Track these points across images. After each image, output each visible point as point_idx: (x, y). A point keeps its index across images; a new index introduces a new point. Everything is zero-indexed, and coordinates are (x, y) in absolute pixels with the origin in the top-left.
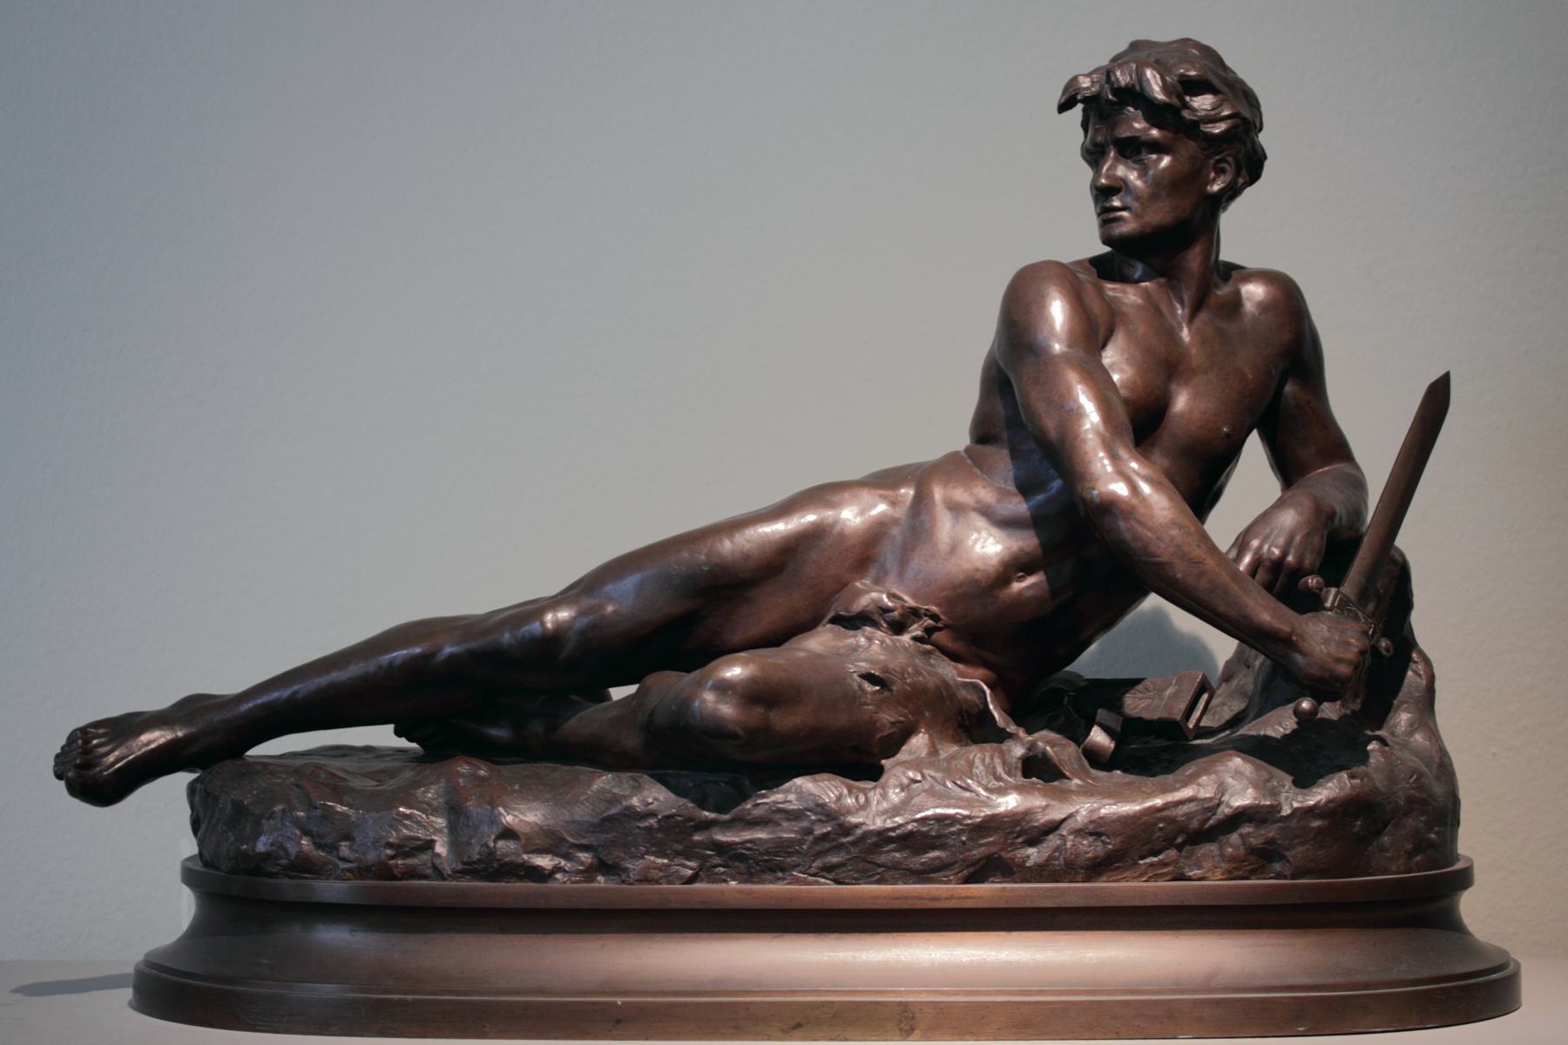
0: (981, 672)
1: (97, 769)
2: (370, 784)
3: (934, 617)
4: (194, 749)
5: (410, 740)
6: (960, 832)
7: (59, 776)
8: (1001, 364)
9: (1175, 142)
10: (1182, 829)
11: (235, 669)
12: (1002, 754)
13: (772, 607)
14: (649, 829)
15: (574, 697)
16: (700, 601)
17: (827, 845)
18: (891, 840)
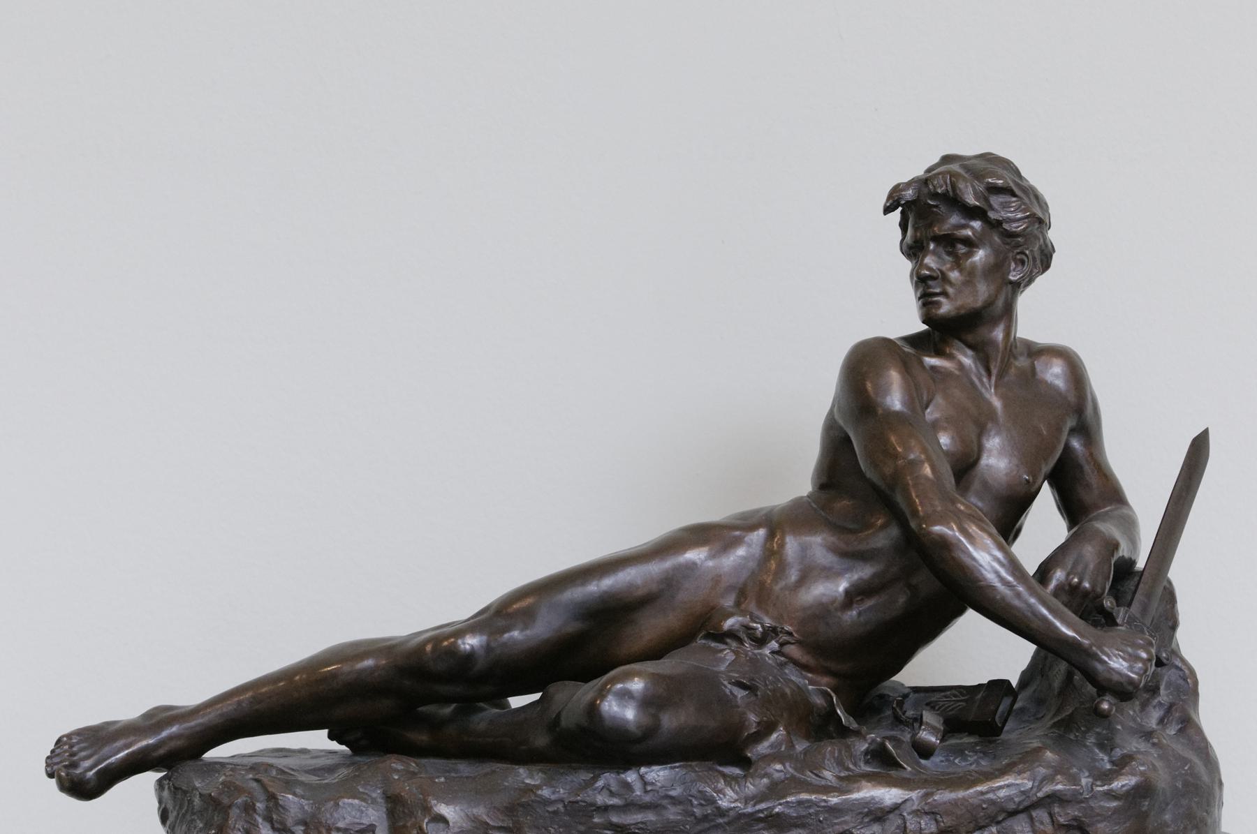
0: (825, 680)
1: (84, 768)
2: (313, 779)
3: (790, 634)
4: (161, 751)
5: (341, 743)
6: (817, 813)
7: (51, 775)
8: (841, 422)
9: (969, 225)
10: (1003, 810)
11: (196, 684)
12: (848, 747)
13: (651, 627)
14: (556, 813)
15: (482, 704)
16: (585, 628)
17: (707, 825)
18: (760, 820)
